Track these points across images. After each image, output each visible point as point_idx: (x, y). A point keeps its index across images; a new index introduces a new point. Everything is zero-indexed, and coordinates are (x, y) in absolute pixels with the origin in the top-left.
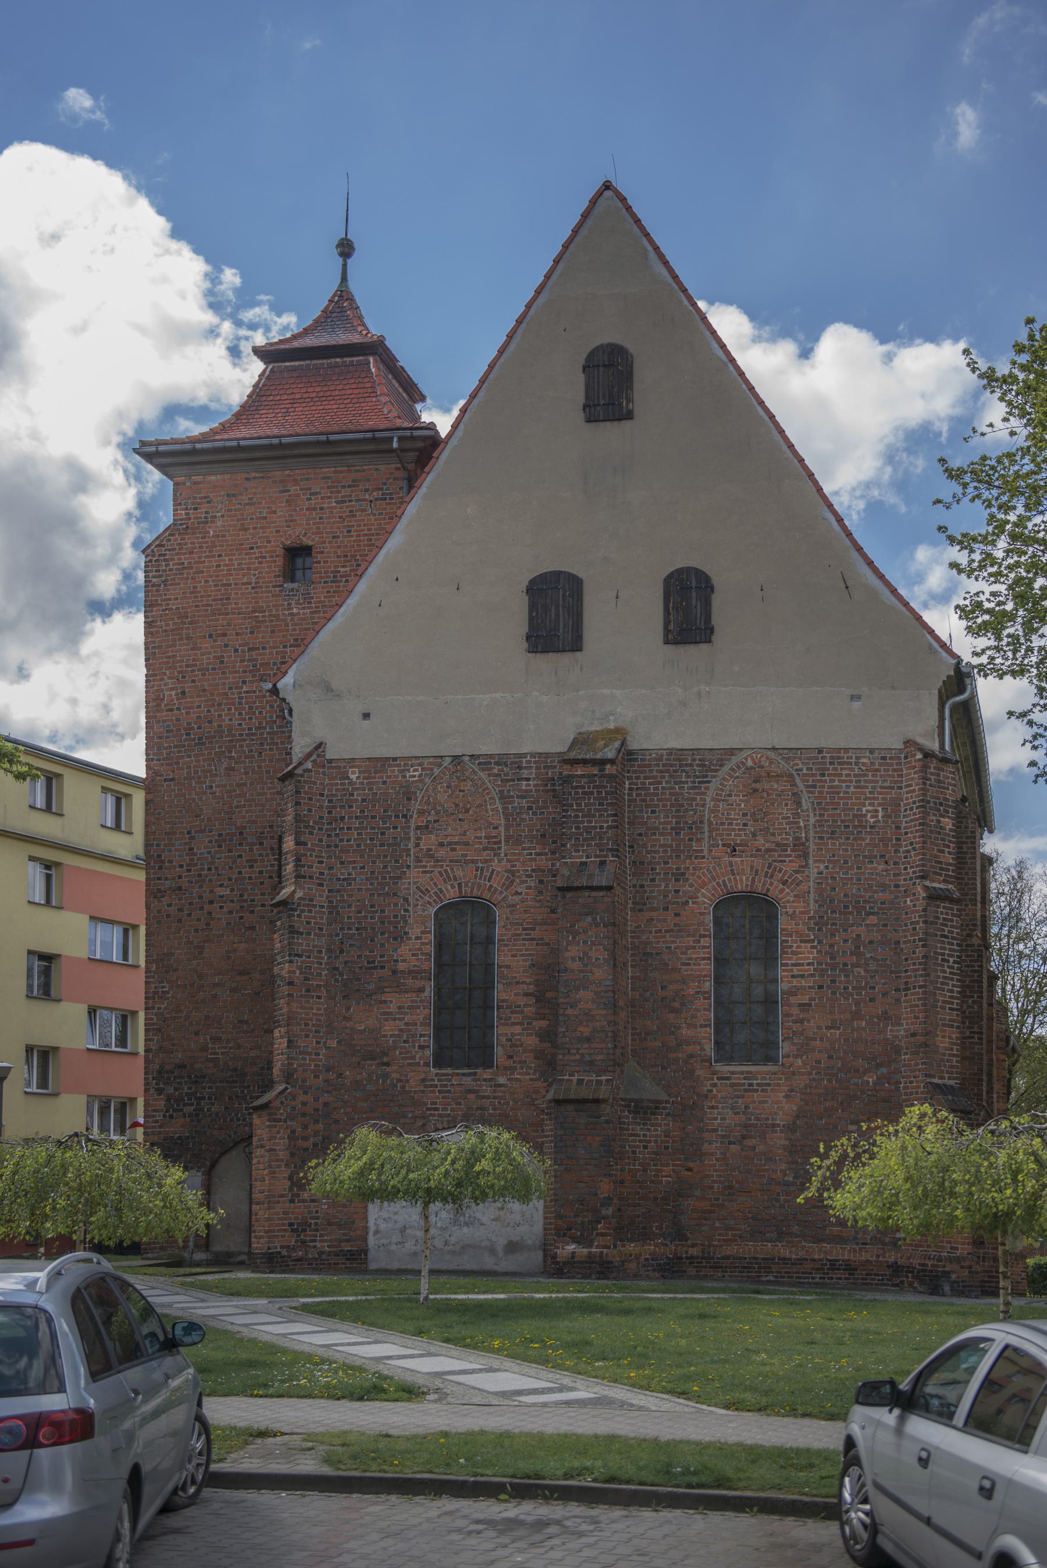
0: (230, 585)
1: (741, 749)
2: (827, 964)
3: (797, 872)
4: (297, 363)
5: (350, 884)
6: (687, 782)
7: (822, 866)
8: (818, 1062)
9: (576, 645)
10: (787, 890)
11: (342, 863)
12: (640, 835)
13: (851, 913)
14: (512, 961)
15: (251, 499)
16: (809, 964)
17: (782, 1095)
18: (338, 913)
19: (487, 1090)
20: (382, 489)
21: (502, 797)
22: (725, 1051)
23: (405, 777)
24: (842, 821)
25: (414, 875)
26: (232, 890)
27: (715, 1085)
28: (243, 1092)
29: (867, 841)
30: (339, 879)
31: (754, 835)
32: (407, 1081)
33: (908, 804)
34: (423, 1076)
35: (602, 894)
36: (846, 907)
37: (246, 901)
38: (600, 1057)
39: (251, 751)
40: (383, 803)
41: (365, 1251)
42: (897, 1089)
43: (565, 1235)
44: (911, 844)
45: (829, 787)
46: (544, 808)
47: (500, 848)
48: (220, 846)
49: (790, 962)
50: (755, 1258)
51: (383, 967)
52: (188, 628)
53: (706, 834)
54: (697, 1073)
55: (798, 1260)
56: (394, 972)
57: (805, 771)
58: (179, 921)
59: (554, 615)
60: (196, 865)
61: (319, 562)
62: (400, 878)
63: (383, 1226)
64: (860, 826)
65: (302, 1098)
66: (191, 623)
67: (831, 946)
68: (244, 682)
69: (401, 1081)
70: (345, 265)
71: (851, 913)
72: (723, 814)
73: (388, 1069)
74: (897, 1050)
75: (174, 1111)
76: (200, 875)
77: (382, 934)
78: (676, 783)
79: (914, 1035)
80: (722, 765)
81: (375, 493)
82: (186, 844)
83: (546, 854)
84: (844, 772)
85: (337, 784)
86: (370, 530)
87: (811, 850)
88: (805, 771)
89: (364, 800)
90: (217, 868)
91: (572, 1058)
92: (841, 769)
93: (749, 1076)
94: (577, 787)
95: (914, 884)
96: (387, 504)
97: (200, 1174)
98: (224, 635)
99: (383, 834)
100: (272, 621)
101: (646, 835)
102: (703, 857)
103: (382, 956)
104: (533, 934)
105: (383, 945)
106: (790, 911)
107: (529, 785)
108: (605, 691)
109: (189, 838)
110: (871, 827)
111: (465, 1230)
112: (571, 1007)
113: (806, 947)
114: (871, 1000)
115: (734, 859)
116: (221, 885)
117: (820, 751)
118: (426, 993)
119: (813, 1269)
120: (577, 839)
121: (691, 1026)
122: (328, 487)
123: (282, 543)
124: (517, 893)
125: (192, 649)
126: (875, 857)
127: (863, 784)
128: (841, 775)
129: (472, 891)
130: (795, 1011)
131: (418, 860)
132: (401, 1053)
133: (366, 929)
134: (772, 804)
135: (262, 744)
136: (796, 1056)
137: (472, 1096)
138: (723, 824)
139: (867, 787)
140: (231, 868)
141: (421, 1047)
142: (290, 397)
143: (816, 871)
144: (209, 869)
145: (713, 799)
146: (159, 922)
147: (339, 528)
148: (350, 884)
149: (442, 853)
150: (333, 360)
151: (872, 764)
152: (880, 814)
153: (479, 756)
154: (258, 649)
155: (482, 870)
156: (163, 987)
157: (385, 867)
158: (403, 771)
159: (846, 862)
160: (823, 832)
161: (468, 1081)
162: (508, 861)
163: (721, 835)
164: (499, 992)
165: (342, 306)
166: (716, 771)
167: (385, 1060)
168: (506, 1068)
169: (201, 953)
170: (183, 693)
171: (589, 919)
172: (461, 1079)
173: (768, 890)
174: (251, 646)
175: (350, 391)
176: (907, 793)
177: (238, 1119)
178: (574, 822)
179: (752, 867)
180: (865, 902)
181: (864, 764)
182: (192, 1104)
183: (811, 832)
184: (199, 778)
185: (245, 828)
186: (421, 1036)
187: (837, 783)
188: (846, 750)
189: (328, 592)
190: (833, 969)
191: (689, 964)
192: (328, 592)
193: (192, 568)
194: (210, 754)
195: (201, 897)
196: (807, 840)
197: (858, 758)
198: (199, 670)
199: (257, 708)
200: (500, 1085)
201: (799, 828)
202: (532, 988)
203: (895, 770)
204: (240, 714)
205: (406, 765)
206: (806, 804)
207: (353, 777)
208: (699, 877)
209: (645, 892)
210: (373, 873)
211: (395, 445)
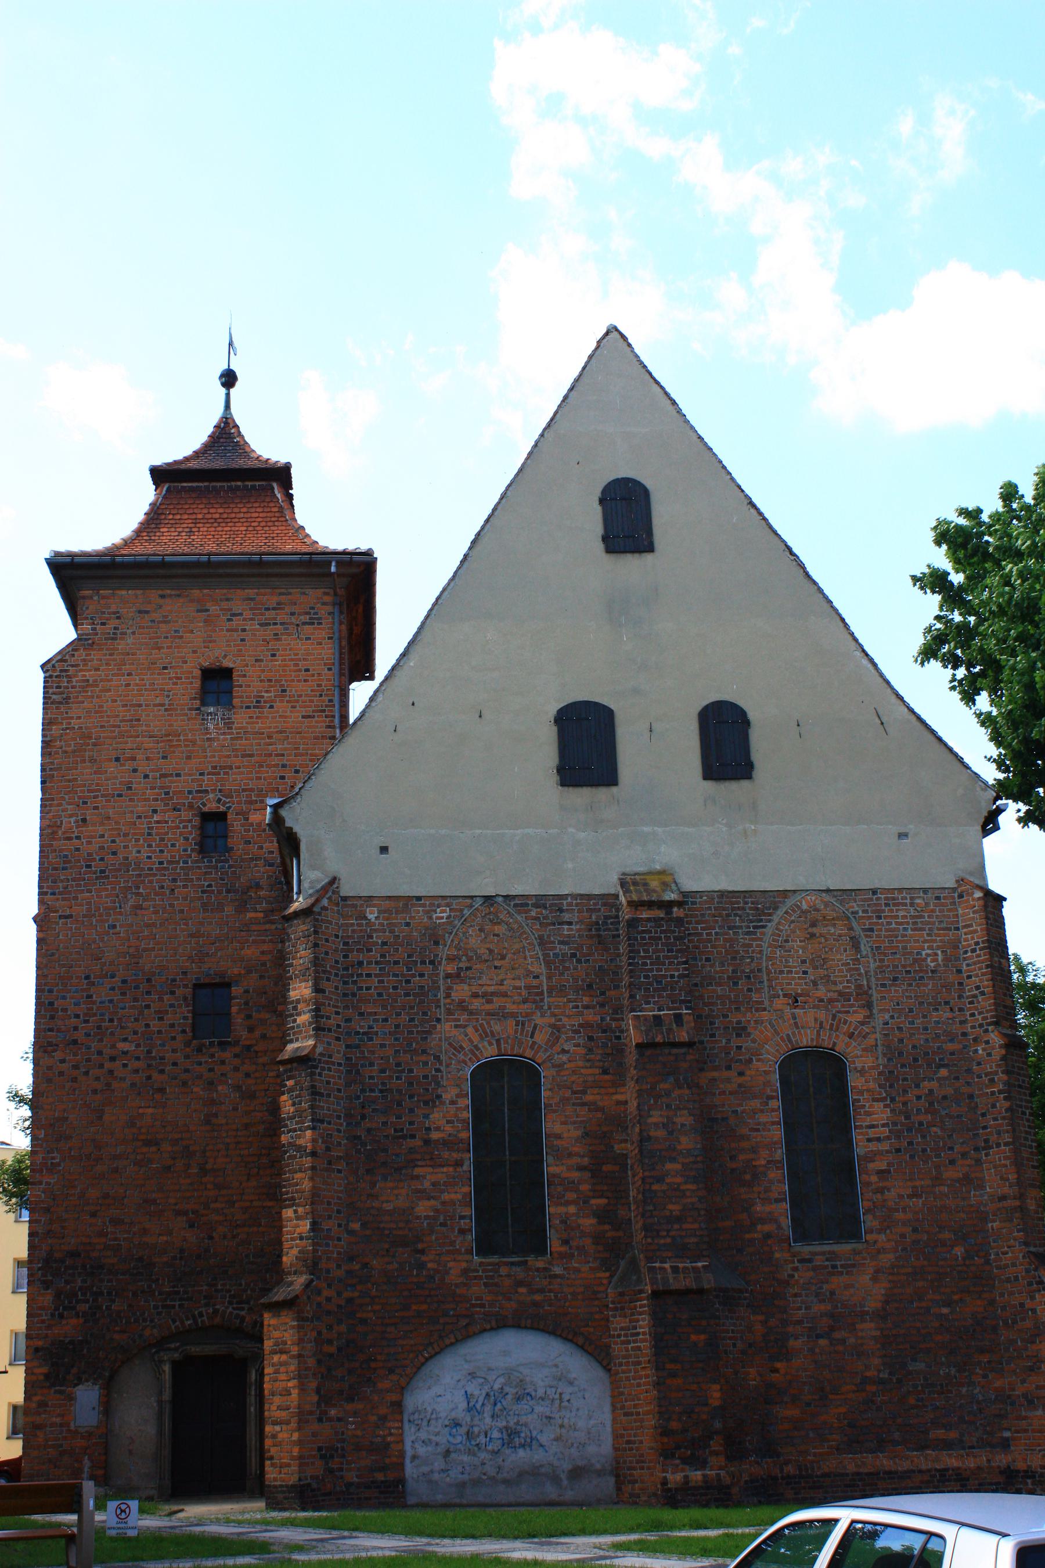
0: (140, 705)
1: (795, 891)
3: (862, 1023)
4: (195, 484)
5: (371, 1039)
6: (741, 927)
7: (887, 1016)
8: (903, 1236)
10: (854, 1044)
11: (361, 1014)
12: (696, 985)
13: (920, 1066)
14: (561, 1127)
15: (166, 617)
16: (883, 1125)
17: (868, 1277)
18: (358, 1072)
20: (310, 613)
21: (542, 942)
23: (431, 918)
24: (904, 966)
25: (446, 1028)
26: (138, 1046)
27: (795, 1269)
28: (150, 1287)
29: (930, 987)
30: (358, 1033)
31: (815, 983)
32: (447, 1273)
33: (969, 945)
34: (464, 1265)
35: (683, 1050)
36: (915, 1060)
37: (154, 1058)
38: (693, 1240)
39: (162, 887)
41: (402, 1481)
42: (987, 1262)
43: (673, 1456)
44: (978, 988)
45: (887, 930)
46: (589, 955)
47: (542, 1000)
48: (124, 994)
49: (864, 1124)
50: (858, 1474)
51: (413, 1137)
52: (92, 750)
53: (766, 983)
54: (777, 1255)
55: (905, 1472)
56: (427, 1142)
57: (861, 914)
58: (74, 1080)
59: (586, 746)
61: (241, 686)
62: (429, 1032)
63: (422, 1450)
64: (921, 971)
65: (326, 1293)
66: (95, 744)
67: (905, 1104)
68: (155, 811)
70: (228, 395)
71: (920, 1066)
72: (781, 961)
73: (424, 1258)
75: (65, 1308)
76: (99, 1027)
77: (411, 1097)
78: (730, 928)
79: (1003, 1198)
80: (776, 908)
81: (302, 617)
82: (83, 990)
83: (594, 1007)
84: (901, 913)
85: (352, 925)
86: (297, 654)
87: (874, 998)
88: (861, 914)
90: (120, 1020)
91: (662, 1241)
92: (897, 910)
93: (832, 1256)
94: (643, 932)
95: (987, 1031)
96: (315, 629)
98: (134, 759)
99: (408, 982)
100: (187, 746)
101: (702, 986)
102: (764, 1009)
103: (411, 1123)
104: (589, 1098)
105: (411, 1111)
106: (859, 1065)
107: (572, 930)
108: (646, 829)
109: (87, 984)
110: (933, 972)
111: (521, 1453)
112: (658, 1181)
113: (878, 1106)
115: (797, 1011)
116: (125, 1040)
117: (874, 892)
118: (465, 1168)
119: (922, 1482)
120: (647, 990)
122: (251, 609)
123: (200, 664)
124: (564, 1051)
125: (95, 773)
126: (940, 1004)
127: (920, 925)
128: (897, 917)
129: (512, 1049)
130: (874, 1178)
131: (449, 1012)
132: (437, 1239)
133: (390, 1090)
134: (831, 949)
135: (174, 880)
136: (880, 1231)
137: (522, 1290)
138: (781, 972)
139: (924, 929)
140: (137, 1020)
141: (462, 1232)
142: (191, 517)
143: (881, 1022)
144: (111, 1020)
145: (770, 945)
147: (262, 651)
148: (371, 1039)
149: (477, 1004)
150: (233, 484)
151: (927, 904)
152: (940, 958)
153: (514, 897)
154: (171, 775)
155: (523, 1025)
156: (53, 1158)
157: (412, 1020)
158: (428, 912)
159: (911, 1010)
160: (884, 979)
161: (519, 1272)
162: (553, 1015)
163: (781, 984)
164: (551, 1167)
165: (226, 433)
166: (770, 915)
167: (420, 1246)
169: (100, 1118)
170: (84, 820)
173: (835, 1044)
174: (163, 772)
175: (257, 515)
176: (966, 934)
177: (145, 1320)
178: (642, 971)
179: (816, 1020)
180: (934, 1053)
181: (918, 904)
182: (87, 1301)
183: (873, 979)
184: (101, 915)
185: (154, 974)
186: (462, 1217)
187: (894, 926)
188: (900, 890)
189: (251, 718)
190: (909, 1130)
191: (758, 1130)
192: (251, 718)
193: (97, 686)
194: (114, 889)
195: (100, 1053)
196: (870, 988)
197: (912, 898)
198: (103, 796)
199: (169, 840)
200: (556, 1276)
201: (860, 975)
202: (586, 1161)
203: (950, 910)
204: (150, 846)
205: (432, 905)
206: (864, 949)
207: (371, 917)
208: (762, 1032)
209: (705, 1049)
211: (333, 569)
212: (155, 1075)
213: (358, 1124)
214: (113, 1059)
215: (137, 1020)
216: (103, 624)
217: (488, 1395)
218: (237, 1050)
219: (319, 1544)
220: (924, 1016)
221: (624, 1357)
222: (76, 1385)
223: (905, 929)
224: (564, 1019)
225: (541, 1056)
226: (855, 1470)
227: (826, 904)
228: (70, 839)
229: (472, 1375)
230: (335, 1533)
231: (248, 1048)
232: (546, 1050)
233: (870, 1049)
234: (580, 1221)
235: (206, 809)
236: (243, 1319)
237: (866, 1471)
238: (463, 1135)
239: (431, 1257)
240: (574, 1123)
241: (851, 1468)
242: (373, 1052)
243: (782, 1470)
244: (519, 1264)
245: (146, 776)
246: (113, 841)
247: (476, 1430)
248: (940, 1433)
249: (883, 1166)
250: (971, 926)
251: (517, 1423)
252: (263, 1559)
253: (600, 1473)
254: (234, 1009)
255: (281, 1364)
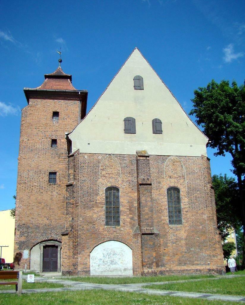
2: (190, 202)
9: (134, 133)
19: (118, 231)
22: (171, 222)
24: (191, 171)
25: (100, 180)
28: (39, 231)
30: (82, 180)
34: (103, 228)
36: (193, 190)
38: (150, 223)
40: (96, 163)
41: (90, 271)
42: (206, 229)
44: (205, 176)
47: (120, 175)
50: (181, 270)
53: (165, 173)
54: (166, 227)
56: (96, 203)
58: (25, 190)
59: (130, 126)
60: (29, 178)
63: (94, 265)
67: (191, 198)
68: (43, 139)
69: (98, 229)
73: (95, 226)
74: (205, 220)
77: (93, 193)
79: (209, 217)
89: (88, 163)
91: (144, 224)
93: (177, 228)
94: (141, 162)
97: (28, 251)
104: (129, 195)
105: (93, 196)
108: (142, 142)
111: (114, 265)
114: (199, 210)
121: (164, 216)
124: (124, 185)
126: (198, 179)
129: (114, 185)
130: (185, 212)
135: (46, 152)
140: (38, 179)
141: (103, 221)
144: (33, 179)
146: (20, 190)
149: (107, 175)
162: (122, 178)
164: (121, 208)
166: (166, 160)
168: (123, 226)
170: (29, 140)
171: (146, 191)
172: (112, 228)
182: (26, 234)
190: (192, 203)
191: (162, 202)
200: (122, 230)
207: (86, 157)
210: (91, 179)
212: (41, 190)
213: (82, 199)
214: (33, 186)
215: (38, 179)
216: (34, 102)
217: (107, 254)
218: (57, 185)
219: (75, 285)
220: (195, 181)
221: (135, 247)
222: (24, 250)
223: (192, 164)
224: (124, 179)
225: (120, 186)
226: (180, 269)
227: (176, 159)
228: (26, 143)
229: (104, 250)
230: (78, 282)
231: (59, 185)
232: (121, 185)
233: (185, 187)
234: (127, 219)
235: (53, 139)
236: (57, 238)
237: (182, 269)
238: (104, 201)
239: (96, 226)
240: (126, 200)
241: (179, 269)
242: (85, 184)
243: (166, 269)
244: (114, 228)
245: (41, 132)
246: (34, 144)
247: (105, 261)
248: (196, 262)
249: (187, 210)
250: (204, 164)
251: (113, 259)
252: (62, 289)
253: (130, 270)
254: (57, 177)
255: (65, 246)
